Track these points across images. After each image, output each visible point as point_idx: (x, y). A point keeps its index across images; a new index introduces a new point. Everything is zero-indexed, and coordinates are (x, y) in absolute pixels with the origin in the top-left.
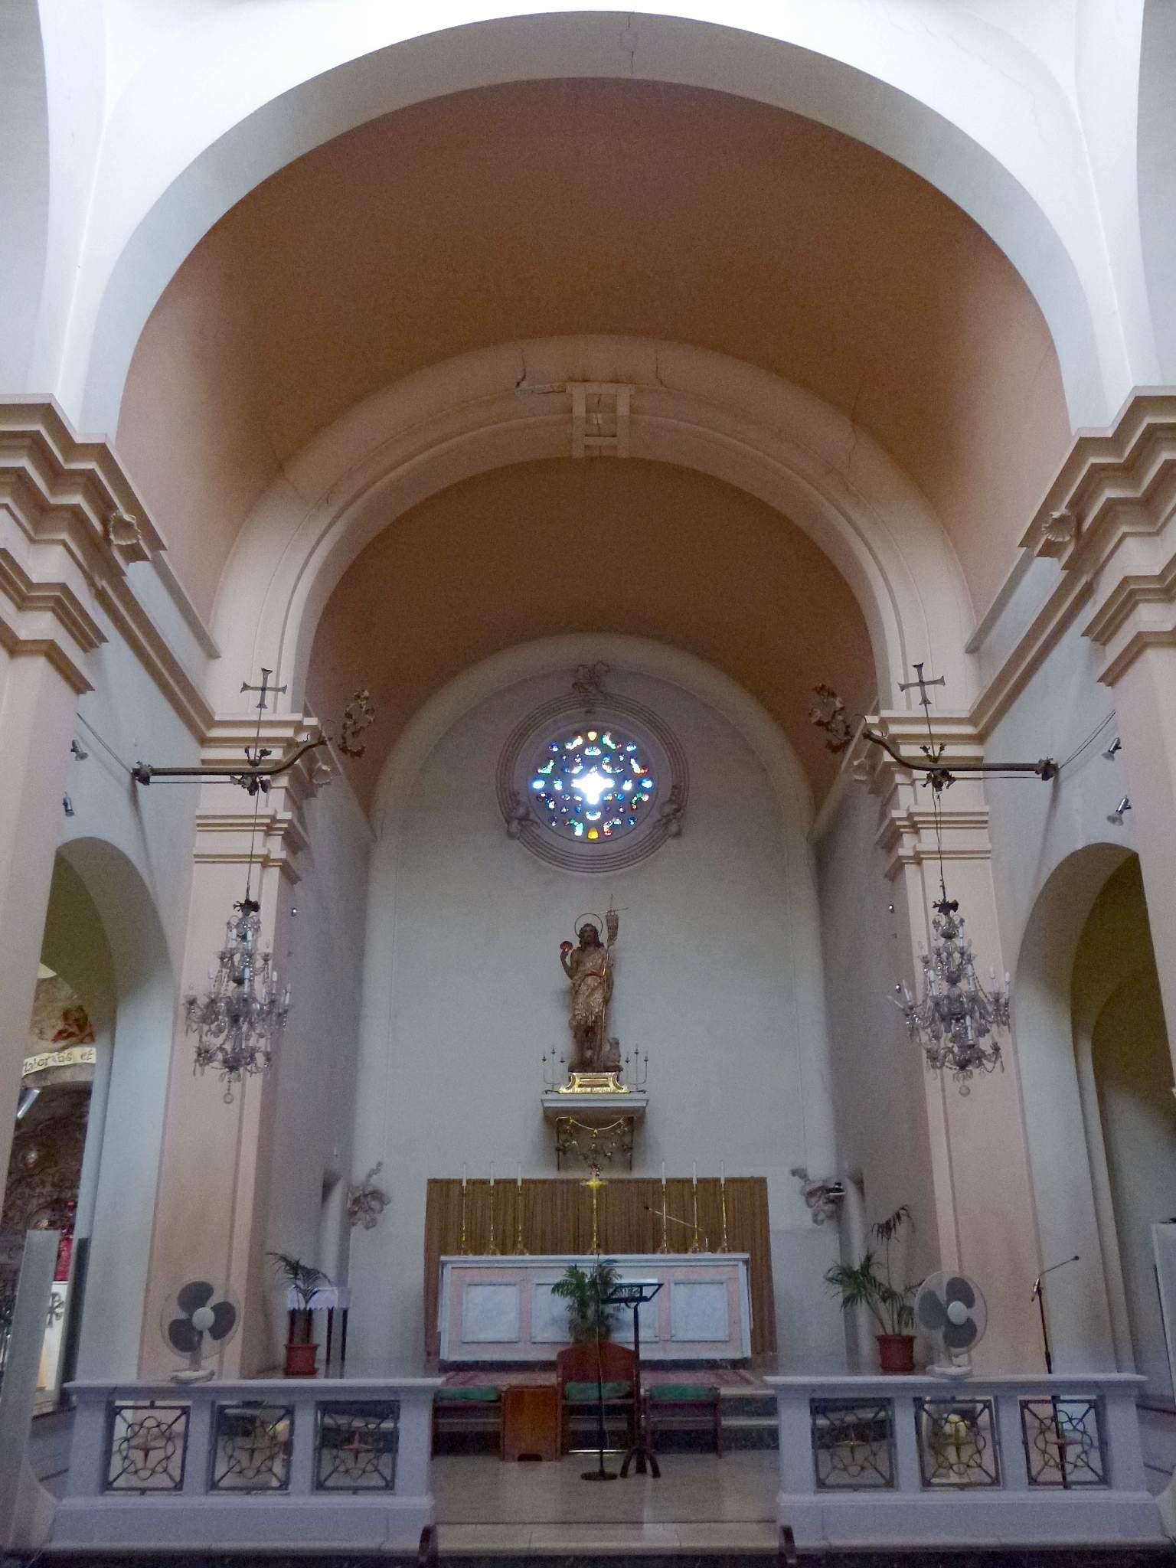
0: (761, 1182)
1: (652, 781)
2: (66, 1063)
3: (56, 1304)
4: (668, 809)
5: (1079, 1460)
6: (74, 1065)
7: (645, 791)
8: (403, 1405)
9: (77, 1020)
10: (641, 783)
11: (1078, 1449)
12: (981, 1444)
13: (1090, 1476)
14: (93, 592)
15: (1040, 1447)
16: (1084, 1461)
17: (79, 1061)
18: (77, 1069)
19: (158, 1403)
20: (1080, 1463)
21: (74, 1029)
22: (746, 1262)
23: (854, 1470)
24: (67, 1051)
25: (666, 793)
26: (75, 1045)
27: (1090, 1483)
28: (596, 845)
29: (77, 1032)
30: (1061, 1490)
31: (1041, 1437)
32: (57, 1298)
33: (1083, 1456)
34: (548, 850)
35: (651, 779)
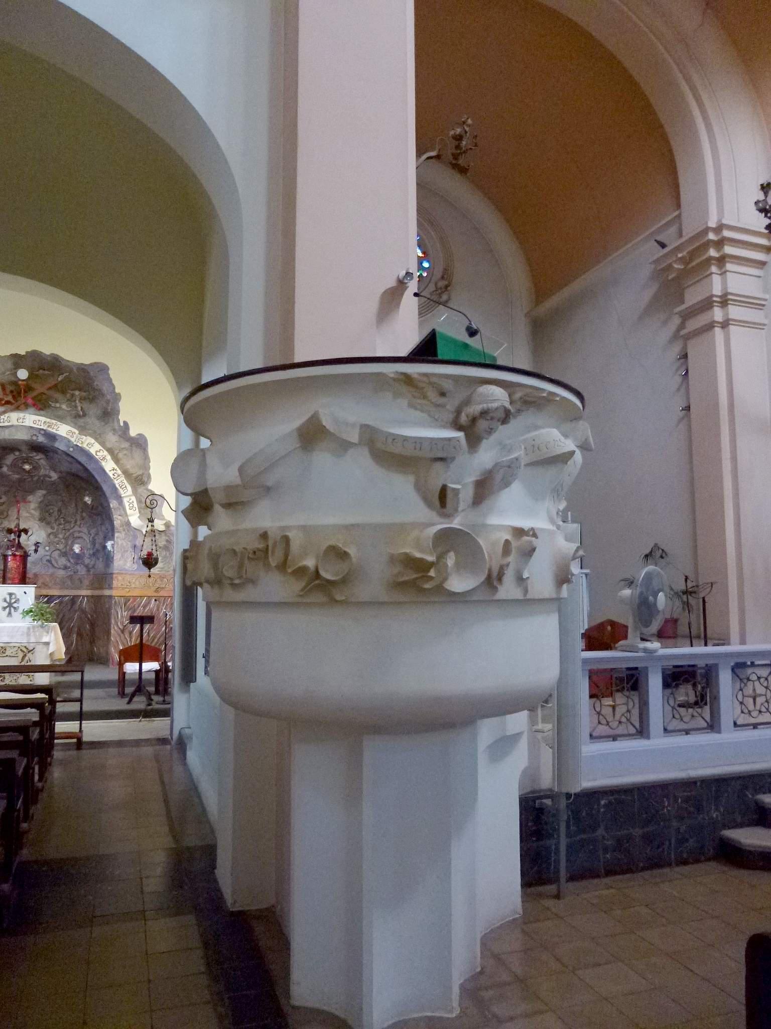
0: (182, 512)
1: (429, 264)
2: (6, 424)
3: (13, 601)
4: (442, 284)
5: (623, 717)
6: (12, 426)
7: (424, 269)
8: (650, 669)
9: (12, 392)
10: (421, 263)
11: (763, 699)
12: (631, 704)
13: (633, 731)
14: (765, 251)
15: (739, 700)
16: (766, 708)
17: (16, 423)
18: (13, 430)
19: (757, 663)
20: (763, 709)
21: (10, 398)
22: (586, 575)
23: (755, 714)
24: (7, 415)
25: (438, 274)
26: (12, 411)
27: (633, 735)
28: (464, 312)
29: (12, 400)
30: (684, 735)
31: (741, 692)
32: (13, 596)
33: (766, 704)
34: (428, 309)
35: (428, 261)
